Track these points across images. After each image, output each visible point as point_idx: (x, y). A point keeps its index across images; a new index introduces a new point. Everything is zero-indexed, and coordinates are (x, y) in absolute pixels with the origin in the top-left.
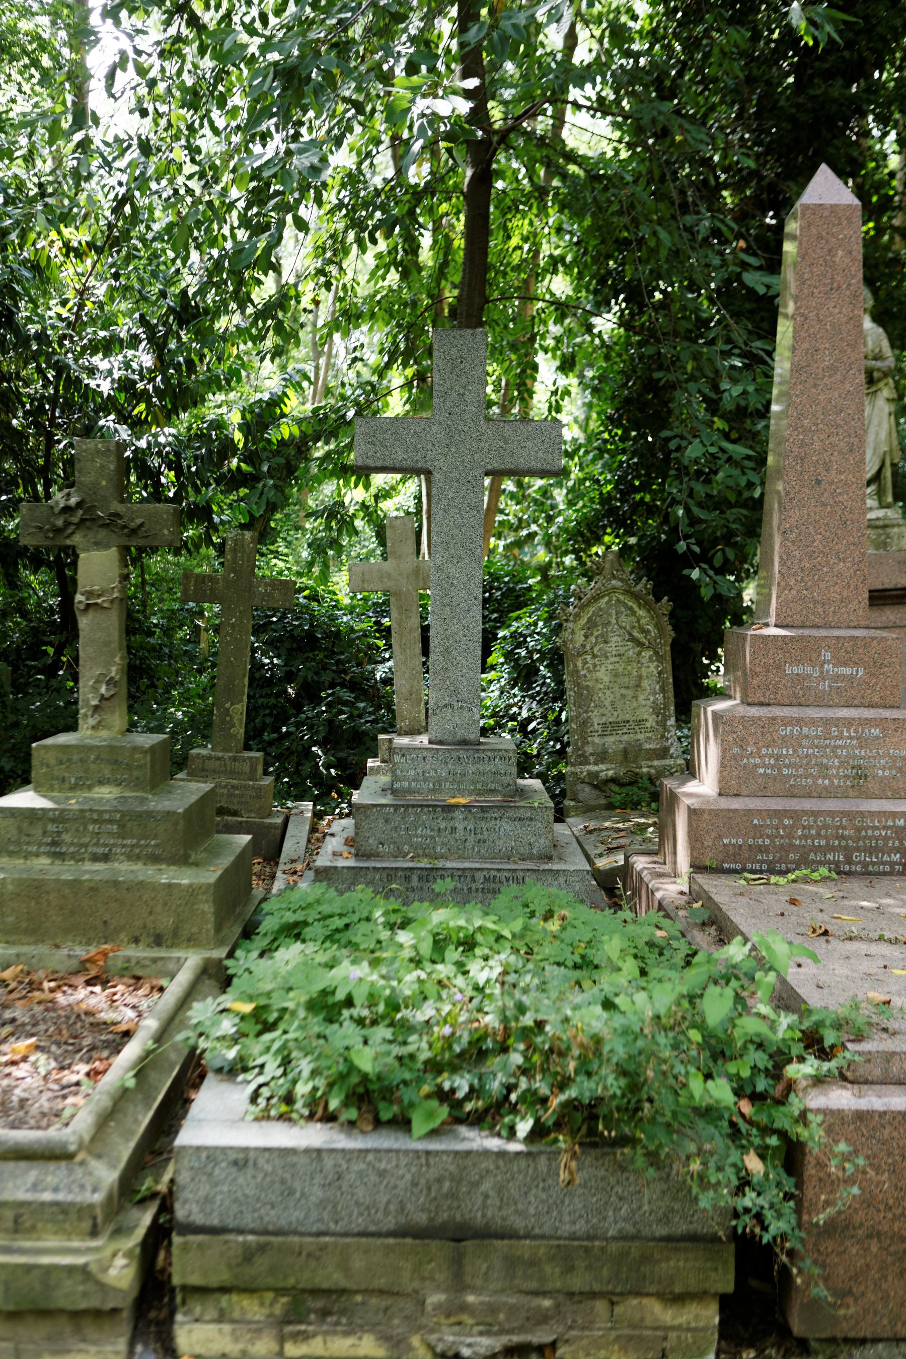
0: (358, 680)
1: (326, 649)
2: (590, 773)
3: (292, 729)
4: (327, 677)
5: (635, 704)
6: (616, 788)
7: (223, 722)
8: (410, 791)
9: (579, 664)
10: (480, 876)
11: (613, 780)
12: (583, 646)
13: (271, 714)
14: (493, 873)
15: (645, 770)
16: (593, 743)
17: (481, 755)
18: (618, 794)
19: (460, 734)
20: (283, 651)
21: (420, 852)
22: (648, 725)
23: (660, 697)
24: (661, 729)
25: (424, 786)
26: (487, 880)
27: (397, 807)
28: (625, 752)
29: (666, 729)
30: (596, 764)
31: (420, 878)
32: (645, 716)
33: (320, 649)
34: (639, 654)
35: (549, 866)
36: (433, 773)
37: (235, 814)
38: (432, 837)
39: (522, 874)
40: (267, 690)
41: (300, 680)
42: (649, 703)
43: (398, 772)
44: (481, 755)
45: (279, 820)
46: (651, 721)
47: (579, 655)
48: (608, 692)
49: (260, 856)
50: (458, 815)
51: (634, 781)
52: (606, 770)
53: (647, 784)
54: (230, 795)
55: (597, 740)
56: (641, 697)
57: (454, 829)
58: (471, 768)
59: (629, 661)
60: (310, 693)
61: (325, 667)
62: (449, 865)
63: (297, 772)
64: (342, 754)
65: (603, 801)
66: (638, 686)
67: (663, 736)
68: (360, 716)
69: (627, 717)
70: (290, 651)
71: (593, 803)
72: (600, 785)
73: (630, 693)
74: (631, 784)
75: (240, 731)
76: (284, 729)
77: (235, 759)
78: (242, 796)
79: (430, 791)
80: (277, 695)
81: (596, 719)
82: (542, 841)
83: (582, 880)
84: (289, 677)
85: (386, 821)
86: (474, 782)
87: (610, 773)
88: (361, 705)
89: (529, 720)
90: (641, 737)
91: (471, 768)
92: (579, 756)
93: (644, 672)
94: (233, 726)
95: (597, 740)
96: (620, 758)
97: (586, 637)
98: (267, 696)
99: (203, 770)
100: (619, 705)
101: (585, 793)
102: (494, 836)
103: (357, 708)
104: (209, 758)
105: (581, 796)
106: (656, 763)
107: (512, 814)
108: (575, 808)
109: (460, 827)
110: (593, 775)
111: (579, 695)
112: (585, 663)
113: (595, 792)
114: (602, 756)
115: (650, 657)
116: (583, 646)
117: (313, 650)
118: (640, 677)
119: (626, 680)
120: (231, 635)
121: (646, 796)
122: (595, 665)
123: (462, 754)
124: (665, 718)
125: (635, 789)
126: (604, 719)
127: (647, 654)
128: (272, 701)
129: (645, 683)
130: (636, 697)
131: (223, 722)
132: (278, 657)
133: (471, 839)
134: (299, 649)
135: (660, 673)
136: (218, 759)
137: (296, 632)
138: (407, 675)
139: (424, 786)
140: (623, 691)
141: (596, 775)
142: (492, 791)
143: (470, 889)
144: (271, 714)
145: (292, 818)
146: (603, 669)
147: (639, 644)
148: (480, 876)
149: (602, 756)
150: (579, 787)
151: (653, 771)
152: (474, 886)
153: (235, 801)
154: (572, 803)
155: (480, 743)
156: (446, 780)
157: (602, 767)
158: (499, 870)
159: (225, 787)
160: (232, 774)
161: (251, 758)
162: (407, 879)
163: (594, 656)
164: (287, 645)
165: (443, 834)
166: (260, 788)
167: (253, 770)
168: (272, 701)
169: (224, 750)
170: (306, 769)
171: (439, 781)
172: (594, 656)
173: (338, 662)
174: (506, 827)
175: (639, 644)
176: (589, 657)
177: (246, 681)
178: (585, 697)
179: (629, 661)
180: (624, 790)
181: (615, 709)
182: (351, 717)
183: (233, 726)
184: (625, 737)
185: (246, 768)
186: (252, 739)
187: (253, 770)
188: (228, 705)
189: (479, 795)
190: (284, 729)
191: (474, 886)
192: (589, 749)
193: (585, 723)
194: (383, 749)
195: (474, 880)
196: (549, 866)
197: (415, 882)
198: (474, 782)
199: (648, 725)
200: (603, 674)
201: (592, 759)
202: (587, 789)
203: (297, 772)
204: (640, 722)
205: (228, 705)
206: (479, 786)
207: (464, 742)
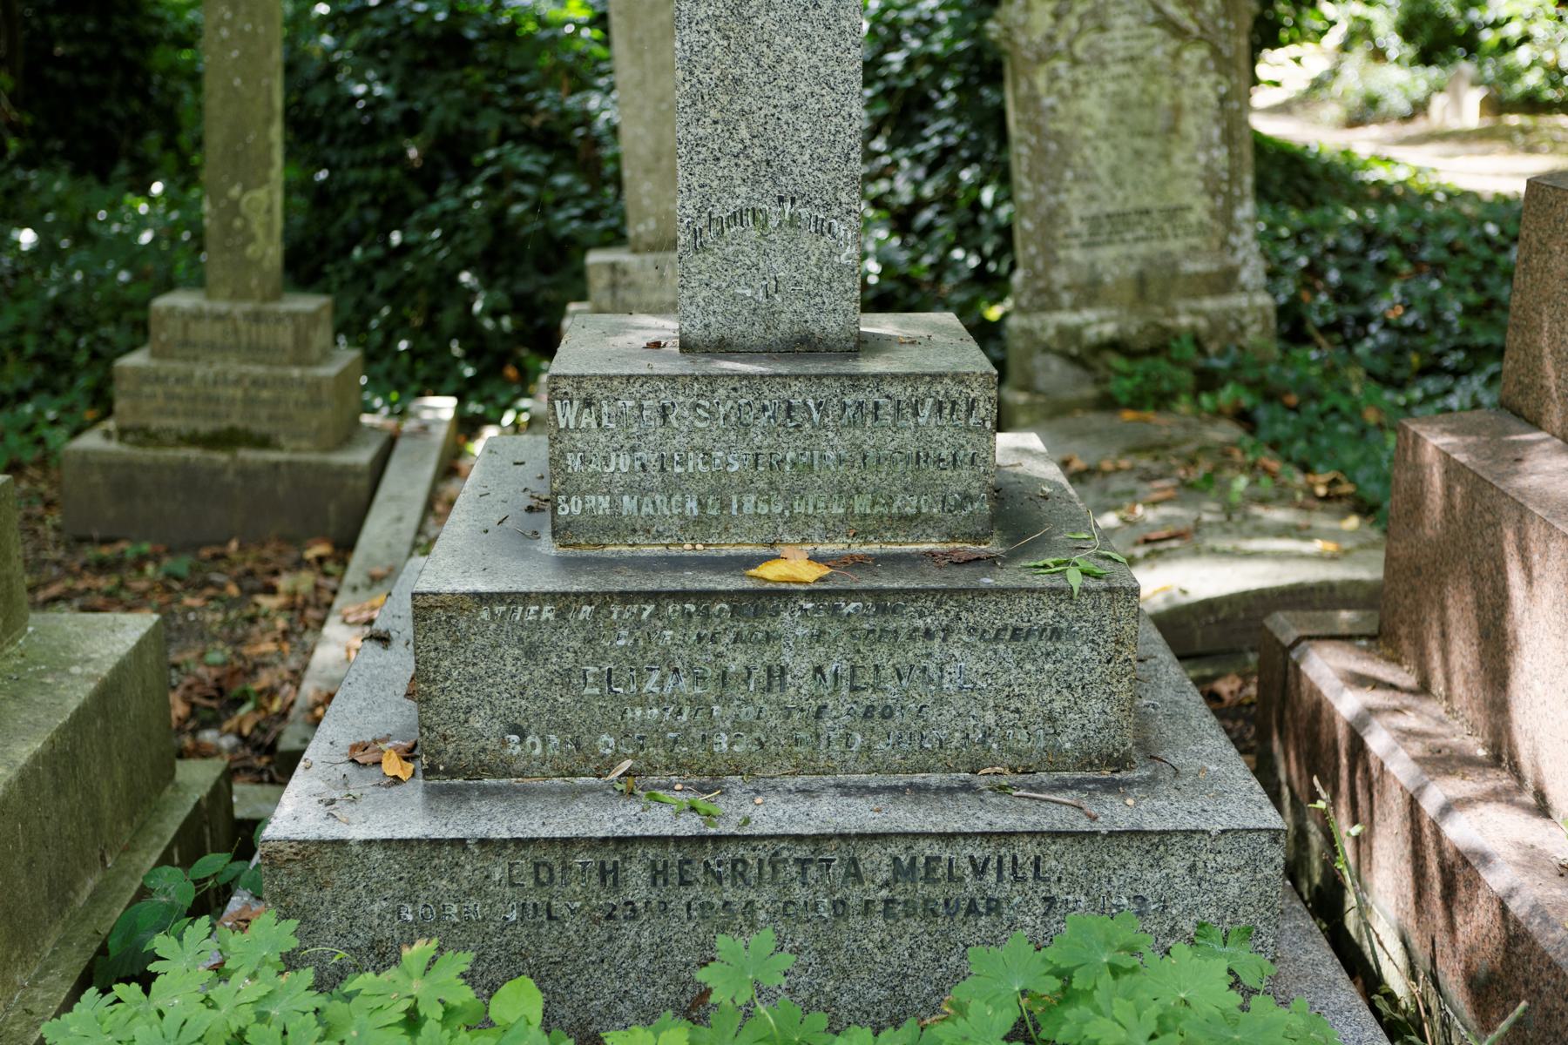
0: (559, 126)
1: (489, 63)
2: (1062, 331)
3: (413, 237)
4: (489, 122)
5: (1164, 172)
6: (1119, 362)
7: (227, 230)
8: (615, 527)
9: (1041, 81)
10: (877, 860)
11: (1116, 345)
12: (1050, 38)
13: (373, 203)
14: (926, 848)
15: (1184, 321)
16: (1070, 263)
17: (869, 397)
18: (1124, 377)
19: (791, 316)
20: (397, 70)
21: (658, 754)
22: (1192, 218)
23: (1220, 155)
24: (1220, 228)
25: (665, 508)
26: (901, 872)
27: (564, 602)
28: (1141, 281)
29: (1231, 226)
30: (1075, 308)
31: (657, 874)
32: (1188, 199)
33: (478, 64)
34: (1176, 55)
35: (1119, 812)
36: (695, 463)
37: (264, 442)
38: (697, 703)
39: (1031, 848)
40: (361, 153)
41: (430, 128)
42: (1196, 169)
43: (574, 463)
44: (869, 397)
45: (362, 456)
46: (1200, 209)
47: (1041, 59)
48: (1104, 146)
49: (323, 537)
50: (791, 623)
51: (1161, 345)
52: (1099, 323)
53: (1190, 352)
54: (249, 401)
55: (1077, 255)
56: (1179, 157)
57: (776, 675)
58: (834, 443)
59: (1154, 73)
60: (455, 155)
61: (488, 101)
62: (771, 814)
63: (430, 326)
64: (522, 287)
65: (1090, 391)
66: (1173, 129)
67: (1224, 243)
68: (558, 204)
69: (1147, 201)
70: (413, 67)
71: (1069, 394)
72: (1084, 356)
73: (1155, 146)
74: (1153, 352)
75: (270, 251)
76: (396, 238)
77: (257, 317)
78: (277, 402)
79: (686, 523)
80: (387, 162)
81: (1076, 206)
82: (1094, 706)
83: (1253, 864)
84: (411, 123)
85: (531, 652)
86: (844, 492)
87: (1109, 330)
88: (562, 180)
89: (918, 204)
90: (1176, 245)
91: (834, 443)
92: (1039, 292)
93: (1187, 97)
94: (251, 239)
95: (1077, 255)
96: (1129, 294)
97: (1057, 16)
98: (365, 164)
99: (186, 343)
100: (1129, 174)
101: (1053, 373)
102: (921, 693)
103: (554, 188)
104: (198, 316)
105: (1042, 382)
106: (1209, 304)
107: (986, 615)
108: (1030, 407)
109: (800, 665)
110: (1070, 335)
111: (1040, 152)
112: (1054, 77)
113: (1073, 372)
114: (1090, 292)
115: (1203, 63)
116: (1050, 38)
117: (461, 65)
118: (1177, 110)
119: (1146, 116)
120: (230, 24)
121: (1185, 377)
122: (1076, 84)
123: (798, 393)
124: (1231, 202)
125: (1162, 364)
126: (1094, 208)
127: (1194, 55)
128: (376, 174)
129: (1189, 124)
130: (1166, 156)
131: (227, 230)
132: (385, 80)
133: (840, 705)
134: (432, 64)
135: (1222, 100)
136: (219, 318)
137: (421, 27)
138: (648, 114)
139: (665, 508)
140: (1140, 143)
141: (1074, 334)
142: (909, 522)
143: (840, 908)
144: (373, 203)
145: (402, 445)
146: (1094, 93)
147: (1177, 31)
148: (877, 860)
149: (1090, 292)
150: (1039, 360)
151: (1202, 323)
152: (855, 895)
153: (263, 413)
154: (1021, 398)
155: (863, 345)
156: (746, 486)
157: (1089, 315)
158: (948, 837)
159: (238, 382)
160: (254, 351)
161: (293, 316)
162: (610, 876)
163: (1075, 62)
164: (405, 53)
165: (738, 691)
166: (317, 384)
167: (302, 342)
168: (376, 174)
169: (235, 296)
170: (449, 318)
171: (720, 490)
172: (1075, 62)
173: (516, 91)
174: (965, 660)
175: (1177, 31)
176: (1061, 66)
177: (276, 132)
178: (1056, 155)
179: (1154, 73)
180: (1141, 366)
181: (1120, 185)
182: (538, 207)
183: (251, 239)
184: (1142, 248)
185: (285, 336)
186: (302, 268)
187: (302, 342)
188: (235, 192)
189: (861, 535)
190: (396, 238)
191: (855, 895)
192: (1060, 276)
193: (1052, 218)
194: (598, 283)
195: (854, 873)
196: (1119, 812)
197: (637, 886)
198: (844, 492)
199: (1192, 218)
200: (1094, 105)
201: (1066, 298)
202: (1055, 364)
203: (430, 326)
204: (1173, 213)
205: (235, 192)
206: (861, 505)
207: (804, 346)
